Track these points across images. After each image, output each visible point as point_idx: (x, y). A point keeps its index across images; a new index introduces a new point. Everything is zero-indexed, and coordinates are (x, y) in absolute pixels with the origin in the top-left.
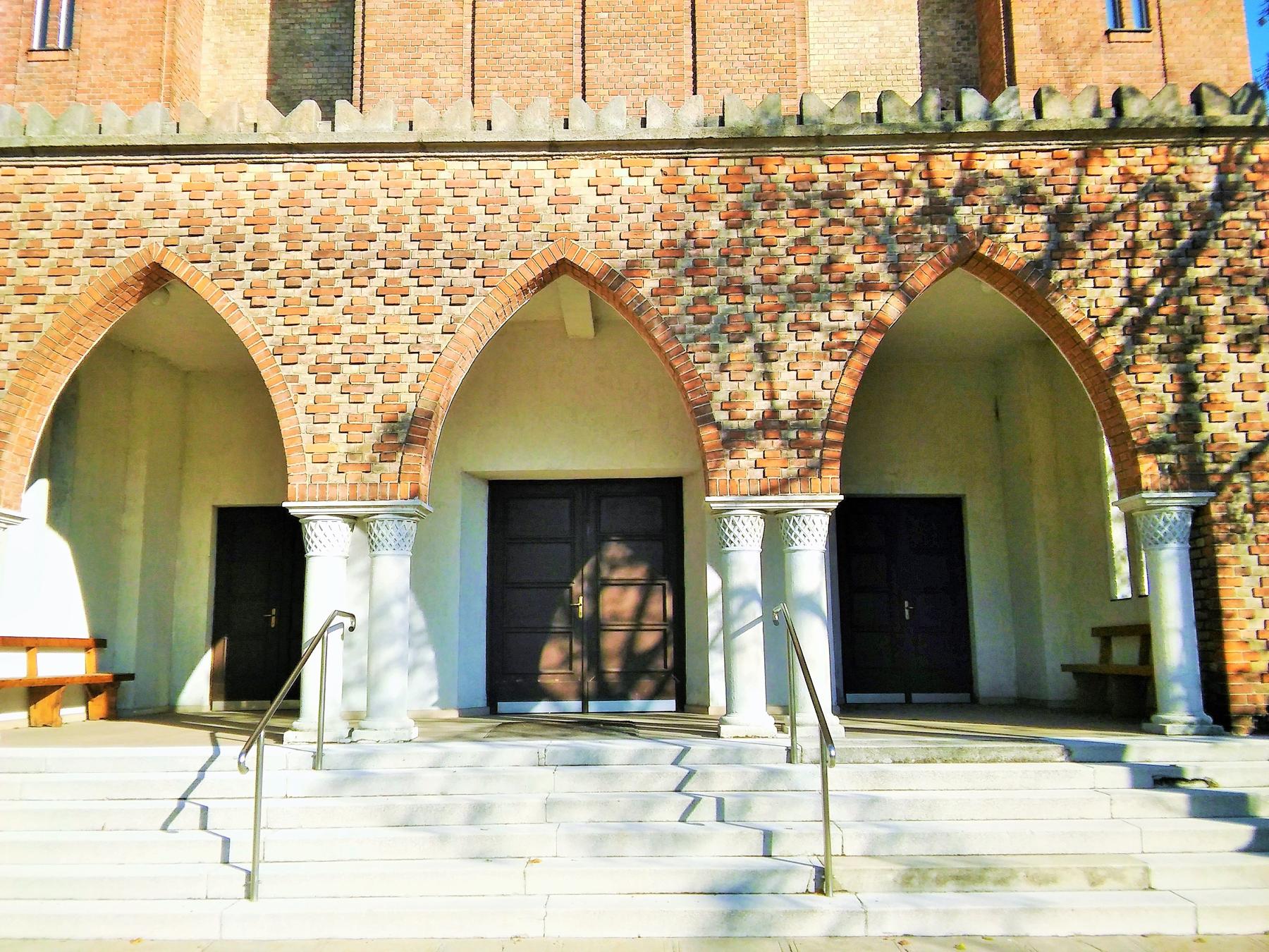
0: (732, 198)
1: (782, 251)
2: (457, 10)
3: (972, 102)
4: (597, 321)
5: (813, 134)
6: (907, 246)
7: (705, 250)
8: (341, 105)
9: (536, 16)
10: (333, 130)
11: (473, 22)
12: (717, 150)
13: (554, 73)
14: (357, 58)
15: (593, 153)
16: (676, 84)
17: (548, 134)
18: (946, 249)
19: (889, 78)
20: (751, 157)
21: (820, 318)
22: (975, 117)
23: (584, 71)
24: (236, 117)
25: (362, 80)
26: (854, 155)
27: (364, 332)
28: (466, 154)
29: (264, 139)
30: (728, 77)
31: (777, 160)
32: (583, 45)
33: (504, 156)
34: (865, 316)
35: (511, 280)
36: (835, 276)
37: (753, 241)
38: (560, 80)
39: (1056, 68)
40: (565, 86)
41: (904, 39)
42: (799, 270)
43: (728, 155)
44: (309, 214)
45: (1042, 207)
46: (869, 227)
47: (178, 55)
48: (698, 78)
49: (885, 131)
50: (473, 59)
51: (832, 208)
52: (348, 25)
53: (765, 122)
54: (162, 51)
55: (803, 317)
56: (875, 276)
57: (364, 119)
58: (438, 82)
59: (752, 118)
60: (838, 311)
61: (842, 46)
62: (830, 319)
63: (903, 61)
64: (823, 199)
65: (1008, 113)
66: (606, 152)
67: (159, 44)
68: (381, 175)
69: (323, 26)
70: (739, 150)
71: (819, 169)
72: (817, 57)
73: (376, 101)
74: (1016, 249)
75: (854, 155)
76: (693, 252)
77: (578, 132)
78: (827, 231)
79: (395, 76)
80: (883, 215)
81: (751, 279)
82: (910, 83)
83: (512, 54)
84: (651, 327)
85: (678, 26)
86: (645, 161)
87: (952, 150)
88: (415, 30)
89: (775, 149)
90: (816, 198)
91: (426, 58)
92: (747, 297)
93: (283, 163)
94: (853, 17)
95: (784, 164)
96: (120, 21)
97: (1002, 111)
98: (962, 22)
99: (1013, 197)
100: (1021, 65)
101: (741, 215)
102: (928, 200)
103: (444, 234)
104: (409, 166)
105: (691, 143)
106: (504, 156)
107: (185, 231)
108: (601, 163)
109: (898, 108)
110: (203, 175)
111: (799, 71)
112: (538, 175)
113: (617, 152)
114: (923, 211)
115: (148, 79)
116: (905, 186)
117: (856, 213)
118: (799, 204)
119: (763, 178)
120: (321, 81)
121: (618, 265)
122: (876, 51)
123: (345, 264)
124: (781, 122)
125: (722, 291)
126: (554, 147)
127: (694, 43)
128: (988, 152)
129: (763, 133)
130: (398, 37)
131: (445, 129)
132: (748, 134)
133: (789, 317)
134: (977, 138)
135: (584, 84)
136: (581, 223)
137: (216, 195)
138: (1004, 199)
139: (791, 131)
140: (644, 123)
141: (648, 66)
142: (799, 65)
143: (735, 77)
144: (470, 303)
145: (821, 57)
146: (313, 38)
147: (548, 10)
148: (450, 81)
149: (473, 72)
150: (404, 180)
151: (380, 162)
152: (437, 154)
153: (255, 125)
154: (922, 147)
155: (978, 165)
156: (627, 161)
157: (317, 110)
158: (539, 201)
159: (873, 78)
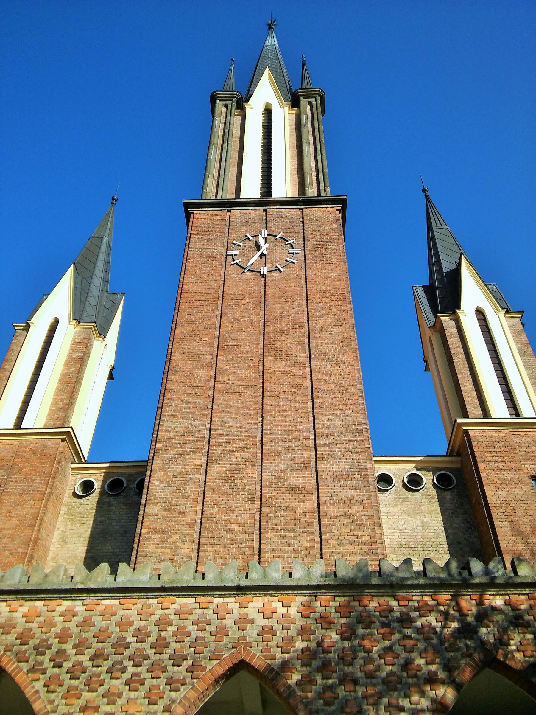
0: (343, 621)
1: (376, 656)
2: (193, 513)
3: (476, 566)
4: (264, 702)
5: (387, 583)
6: (452, 654)
7: (329, 654)
8: (122, 566)
9: (235, 515)
10: (115, 580)
11: (202, 518)
12: (333, 592)
13: (243, 545)
14: (137, 539)
15: (262, 593)
16: (311, 552)
17: (236, 581)
18: (476, 656)
19: (430, 549)
20: (353, 596)
21: (405, 703)
22: (479, 574)
23: (260, 544)
24: (62, 573)
25: (137, 550)
26: (413, 596)
27: (113, 710)
28: (188, 593)
29: (75, 586)
30: (340, 548)
31: (369, 598)
32: (260, 530)
33: (210, 595)
34: (434, 701)
35: (209, 674)
36: (411, 673)
37: (358, 648)
38: (247, 549)
39: (523, 545)
40: (249, 553)
41: (435, 528)
42: (389, 668)
43: (340, 594)
44: (93, 631)
45: (529, 629)
46: (429, 641)
47: (40, 536)
48: (323, 548)
49: (428, 582)
50: (200, 538)
51: (403, 628)
52: (135, 520)
53: (360, 575)
54: (32, 535)
55: (394, 702)
56: (436, 674)
57: (133, 573)
58: (179, 551)
59: (352, 572)
60: (415, 698)
61: (402, 531)
62: (410, 703)
63: (437, 540)
64: (398, 622)
65: (497, 572)
66: (269, 592)
67: (31, 531)
68: (139, 606)
69: (122, 521)
70: (347, 591)
71: (394, 603)
72: (389, 537)
73: (143, 562)
74: (518, 656)
75: (413, 596)
76: (322, 656)
77: (253, 580)
78: (402, 643)
79: (156, 548)
80: (435, 632)
81: (359, 674)
82: (443, 552)
83: (221, 535)
84: (297, 708)
85: (311, 520)
86: (291, 597)
87: (469, 593)
88: (169, 523)
89: (367, 591)
90: (393, 621)
91: (175, 537)
92: (357, 688)
93: (83, 600)
94: (406, 516)
95: (372, 600)
96: (13, 519)
97: (495, 570)
98: (466, 520)
99: (511, 623)
100: (503, 543)
101: (350, 632)
102: (460, 624)
103: (171, 644)
104: (155, 601)
105: (318, 587)
106: (210, 595)
107: (18, 641)
108: (266, 598)
109: (434, 568)
110: (37, 607)
111: (379, 545)
112: (229, 606)
113: (276, 592)
114: (458, 631)
115: (20, 550)
116: (446, 616)
117: (419, 631)
118: (384, 625)
119: (361, 608)
120: (115, 550)
121: (276, 663)
122: (421, 534)
123: (110, 663)
124: (369, 575)
125: (342, 681)
126: (240, 589)
127: (320, 530)
128: (490, 595)
129: (358, 581)
130: (160, 527)
131: (178, 579)
132: (350, 582)
133: (385, 700)
134: (483, 587)
135: (260, 552)
136: (254, 636)
137: (42, 619)
138: (506, 624)
139: (375, 581)
140: (291, 575)
141: (295, 542)
142: (378, 542)
143: (343, 548)
144: (182, 690)
145: (391, 537)
146: (115, 527)
147: (242, 512)
148: (186, 550)
149: (199, 545)
150: (151, 609)
151: (139, 599)
152: (172, 594)
153: (72, 577)
154: (451, 592)
155: (487, 602)
156: (281, 597)
157: (108, 569)
158: (229, 622)
159: (422, 549)
